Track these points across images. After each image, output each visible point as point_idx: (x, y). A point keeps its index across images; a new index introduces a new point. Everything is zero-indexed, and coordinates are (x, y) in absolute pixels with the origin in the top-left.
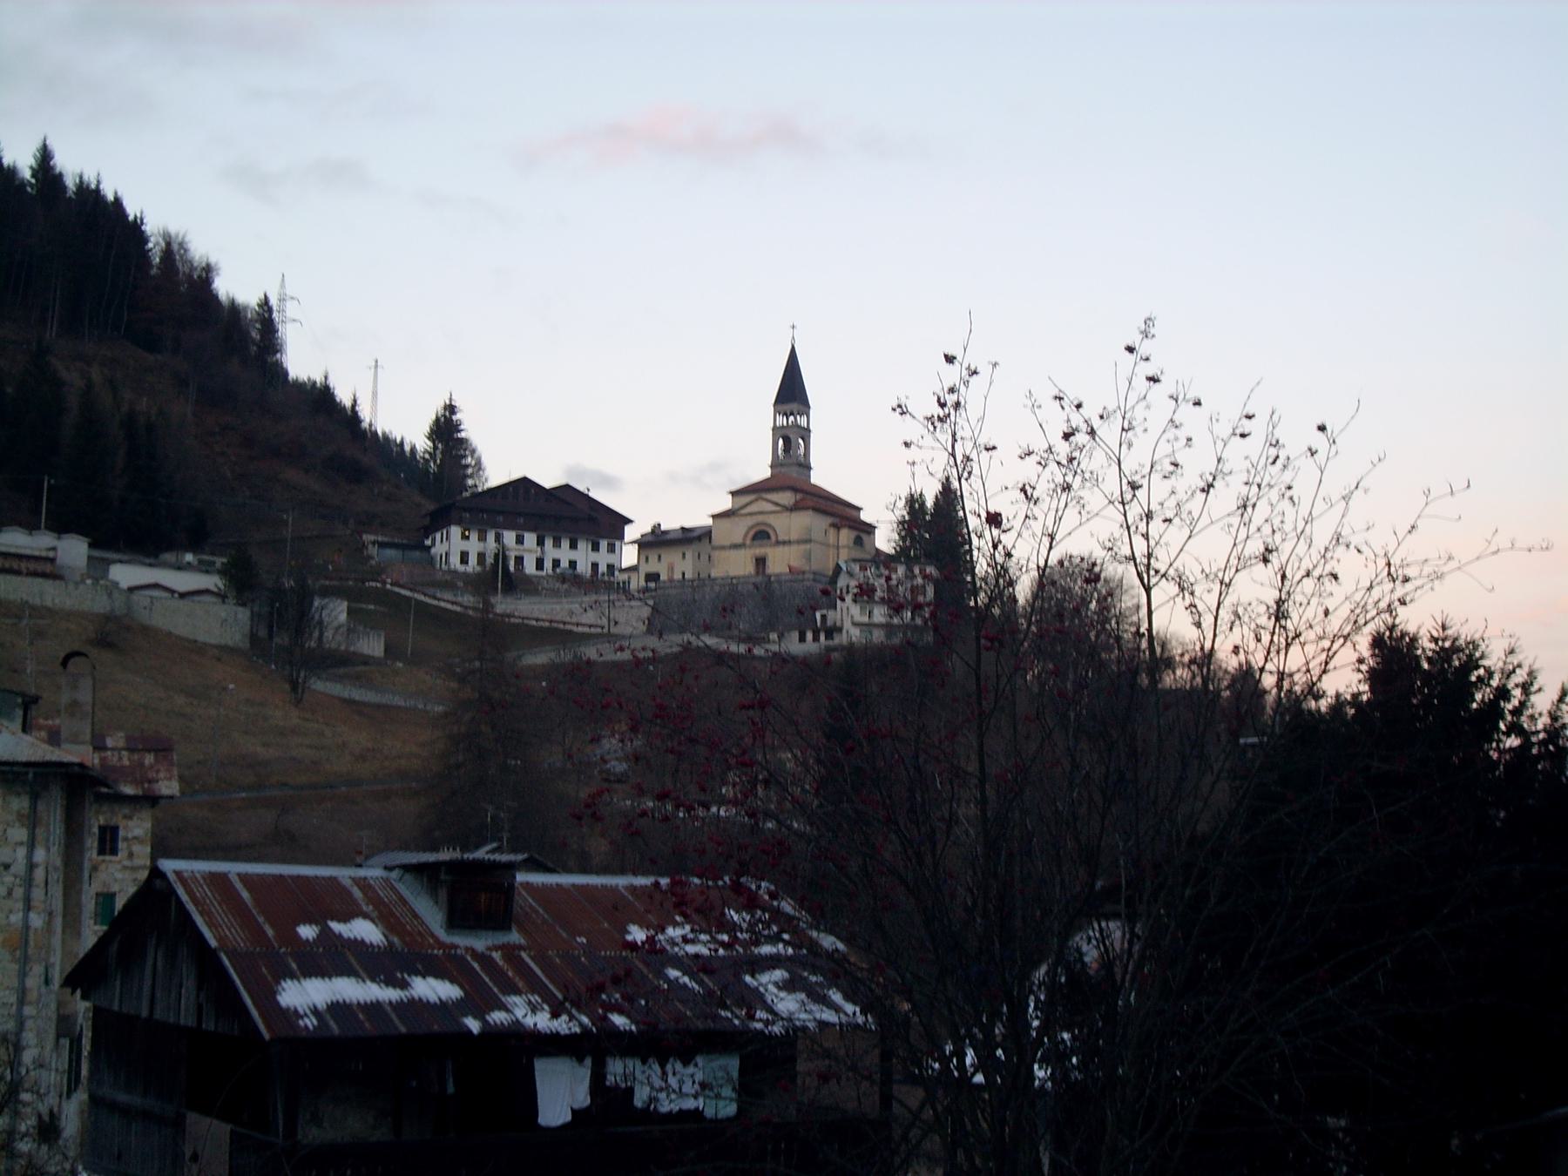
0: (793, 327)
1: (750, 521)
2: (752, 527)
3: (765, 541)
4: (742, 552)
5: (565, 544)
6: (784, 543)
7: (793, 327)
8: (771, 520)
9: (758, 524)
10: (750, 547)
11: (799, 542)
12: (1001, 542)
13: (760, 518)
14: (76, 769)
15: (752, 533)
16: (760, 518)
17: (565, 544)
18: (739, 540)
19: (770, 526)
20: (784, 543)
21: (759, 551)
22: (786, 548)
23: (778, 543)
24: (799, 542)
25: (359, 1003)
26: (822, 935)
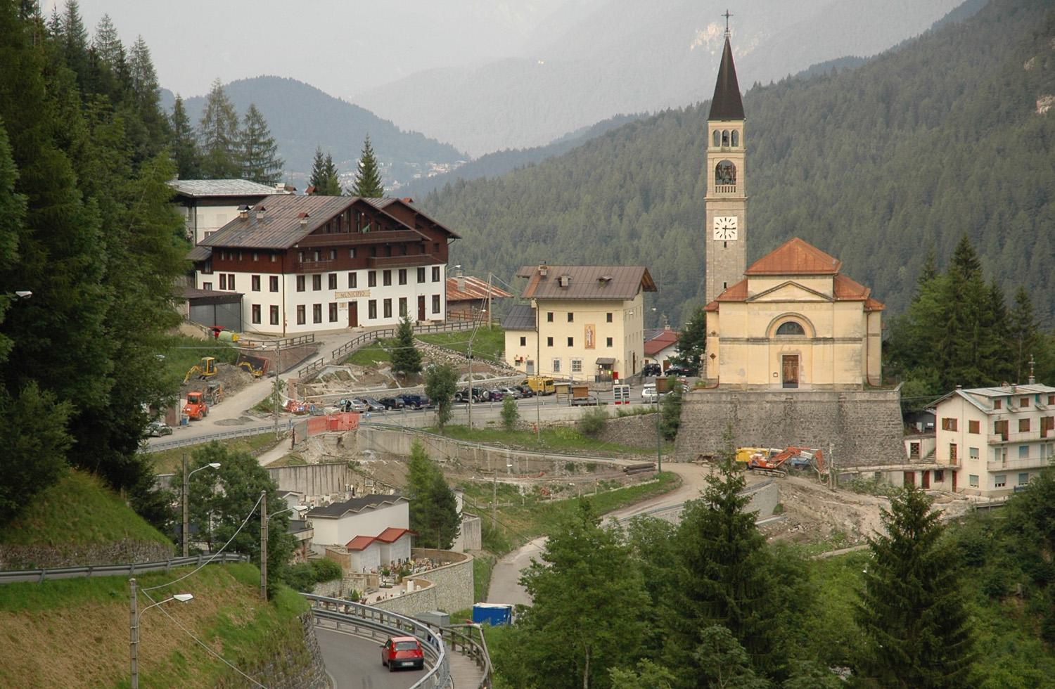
0: (727, 16)
1: (777, 311)
2: (778, 318)
3: (797, 336)
4: (764, 348)
5: (412, 276)
6: (825, 340)
7: (727, 16)
8: (806, 311)
9: (786, 316)
10: (777, 341)
11: (845, 340)
12: (840, 393)
13: (790, 308)
14: (829, 387)
15: (779, 323)
16: (790, 308)
17: (412, 276)
18: (762, 335)
19: (804, 318)
20: (825, 340)
21: (789, 348)
22: (828, 346)
23: (816, 340)
24: (845, 340)
25: (92, 472)
26: (200, 544)
